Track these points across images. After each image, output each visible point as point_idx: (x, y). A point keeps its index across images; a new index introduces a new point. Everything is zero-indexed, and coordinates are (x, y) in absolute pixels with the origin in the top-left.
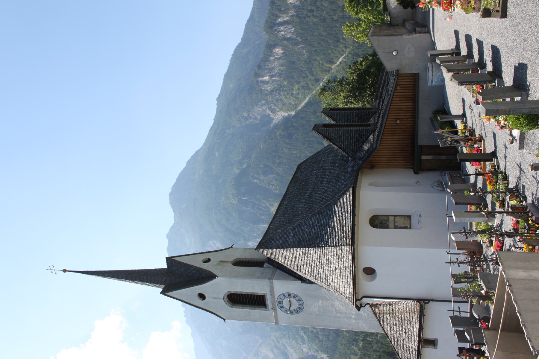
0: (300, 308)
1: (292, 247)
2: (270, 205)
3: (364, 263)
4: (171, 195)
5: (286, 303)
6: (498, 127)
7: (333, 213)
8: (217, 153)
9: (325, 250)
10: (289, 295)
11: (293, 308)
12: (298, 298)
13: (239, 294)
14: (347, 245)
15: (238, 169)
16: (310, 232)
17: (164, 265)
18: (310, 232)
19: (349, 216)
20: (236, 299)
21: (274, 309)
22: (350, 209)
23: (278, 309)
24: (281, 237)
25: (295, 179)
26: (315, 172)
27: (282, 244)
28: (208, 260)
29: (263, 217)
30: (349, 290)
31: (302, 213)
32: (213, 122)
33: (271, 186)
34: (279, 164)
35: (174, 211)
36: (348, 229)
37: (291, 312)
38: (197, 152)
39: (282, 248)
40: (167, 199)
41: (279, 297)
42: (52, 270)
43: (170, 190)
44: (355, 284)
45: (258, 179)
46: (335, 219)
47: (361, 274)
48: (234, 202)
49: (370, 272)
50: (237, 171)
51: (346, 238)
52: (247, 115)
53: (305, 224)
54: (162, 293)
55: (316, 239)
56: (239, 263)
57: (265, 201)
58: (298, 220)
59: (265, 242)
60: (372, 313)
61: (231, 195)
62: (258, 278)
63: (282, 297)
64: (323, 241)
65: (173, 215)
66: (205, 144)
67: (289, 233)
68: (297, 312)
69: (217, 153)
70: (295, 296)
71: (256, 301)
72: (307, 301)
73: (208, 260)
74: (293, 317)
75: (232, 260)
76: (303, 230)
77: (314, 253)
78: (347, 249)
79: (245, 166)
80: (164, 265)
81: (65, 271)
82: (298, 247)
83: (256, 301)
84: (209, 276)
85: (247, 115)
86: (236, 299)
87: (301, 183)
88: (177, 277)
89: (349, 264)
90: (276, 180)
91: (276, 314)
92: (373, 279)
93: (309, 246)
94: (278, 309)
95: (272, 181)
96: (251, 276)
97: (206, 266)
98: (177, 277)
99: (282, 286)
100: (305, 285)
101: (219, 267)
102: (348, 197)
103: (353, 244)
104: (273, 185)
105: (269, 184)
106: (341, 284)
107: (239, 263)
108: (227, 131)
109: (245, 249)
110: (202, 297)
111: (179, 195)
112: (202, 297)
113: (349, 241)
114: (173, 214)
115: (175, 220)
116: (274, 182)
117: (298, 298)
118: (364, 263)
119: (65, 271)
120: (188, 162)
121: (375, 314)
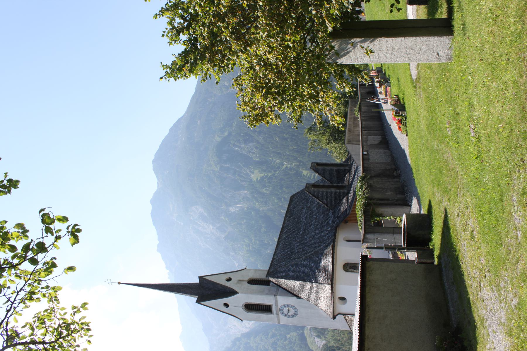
0: (295, 314)
1: (292, 279)
2: (251, 172)
3: (339, 294)
4: (154, 161)
5: (285, 310)
6: (460, 131)
7: (320, 260)
8: (199, 122)
9: (314, 285)
10: (288, 306)
11: (290, 314)
12: (294, 308)
13: (253, 305)
14: (329, 284)
15: (220, 137)
16: (304, 270)
17: (197, 281)
18: (304, 270)
19: (330, 264)
20: (250, 307)
21: (277, 314)
22: (331, 260)
23: (280, 314)
24: (284, 271)
25: (289, 213)
26: (305, 211)
27: (285, 276)
28: (229, 280)
29: (244, 183)
30: (329, 310)
31: (298, 252)
32: (194, 90)
33: (251, 154)
34: (260, 133)
35: (157, 177)
36: (329, 273)
37: (289, 316)
38: (179, 120)
39: (285, 279)
40: (150, 166)
41: (281, 307)
42: (109, 282)
43: (153, 157)
44: (333, 307)
45: (239, 147)
46: (321, 264)
47: (337, 301)
48: (216, 170)
49: (343, 299)
50: (218, 139)
51: (328, 280)
52: (228, 84)
53: (301, 264)
54: (198, 302)
55: (309, 275)
56: (252, 282)
57: (246, 169)
58: (295, 259)
59: (273, 272)
60: (344, 319)
61: (212, 163)
62: (267, 294)
63: (283, 307)
64: (313, 278)
65: (157, 181)
66: (187, 112)
67: (290, 268)
68: (293, 316)
69: (199, 122)
70: (292, 307)
71: (266, 309)
72: (300, 310)
73: (229, 280)
74: (290, 319)
75: (247, 279)
76: (299, 268)
77: (307, 285)
78: (328, 287)
79: (226, 134)
80: (197, 281)
81: (119, 283)
82: (296, 280)
83: (266, 309)
84: (232, 292)
85: (228, 84)
86: (250, 307)
87: (294, 219)
88: (207, 291)
89: (330, 295)
90: (256, 148)
91: (278, 317)
92: (345, 303)
93: (304, 280)
94: (280, 314)
95: (252, 149)
96: (262, 293)
97: (228, 284)
98: (207, 291)
99: (283, 300)
100: (299, 299)
101: (238, 285)
102: (329, 250)
103: (332, 284)
104: (253, 153)
105: (250, 152)
106: (324, 306)
107: (252, 282)
108: (209, 100)
109: (256, 270)
110: (226, 305)
111: (160, 161)
112: (226, 305)
113: (330, 282)
114: (156, 180)
115: (158, 186)
116: (255, 150)
117: (294, 308)
118: (339, 294)
119: (119, 283)
120: (171, 130)
121: (346, 320)
